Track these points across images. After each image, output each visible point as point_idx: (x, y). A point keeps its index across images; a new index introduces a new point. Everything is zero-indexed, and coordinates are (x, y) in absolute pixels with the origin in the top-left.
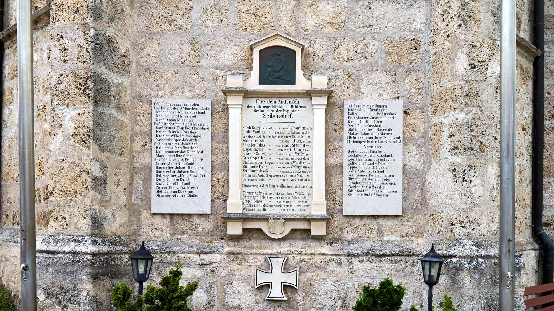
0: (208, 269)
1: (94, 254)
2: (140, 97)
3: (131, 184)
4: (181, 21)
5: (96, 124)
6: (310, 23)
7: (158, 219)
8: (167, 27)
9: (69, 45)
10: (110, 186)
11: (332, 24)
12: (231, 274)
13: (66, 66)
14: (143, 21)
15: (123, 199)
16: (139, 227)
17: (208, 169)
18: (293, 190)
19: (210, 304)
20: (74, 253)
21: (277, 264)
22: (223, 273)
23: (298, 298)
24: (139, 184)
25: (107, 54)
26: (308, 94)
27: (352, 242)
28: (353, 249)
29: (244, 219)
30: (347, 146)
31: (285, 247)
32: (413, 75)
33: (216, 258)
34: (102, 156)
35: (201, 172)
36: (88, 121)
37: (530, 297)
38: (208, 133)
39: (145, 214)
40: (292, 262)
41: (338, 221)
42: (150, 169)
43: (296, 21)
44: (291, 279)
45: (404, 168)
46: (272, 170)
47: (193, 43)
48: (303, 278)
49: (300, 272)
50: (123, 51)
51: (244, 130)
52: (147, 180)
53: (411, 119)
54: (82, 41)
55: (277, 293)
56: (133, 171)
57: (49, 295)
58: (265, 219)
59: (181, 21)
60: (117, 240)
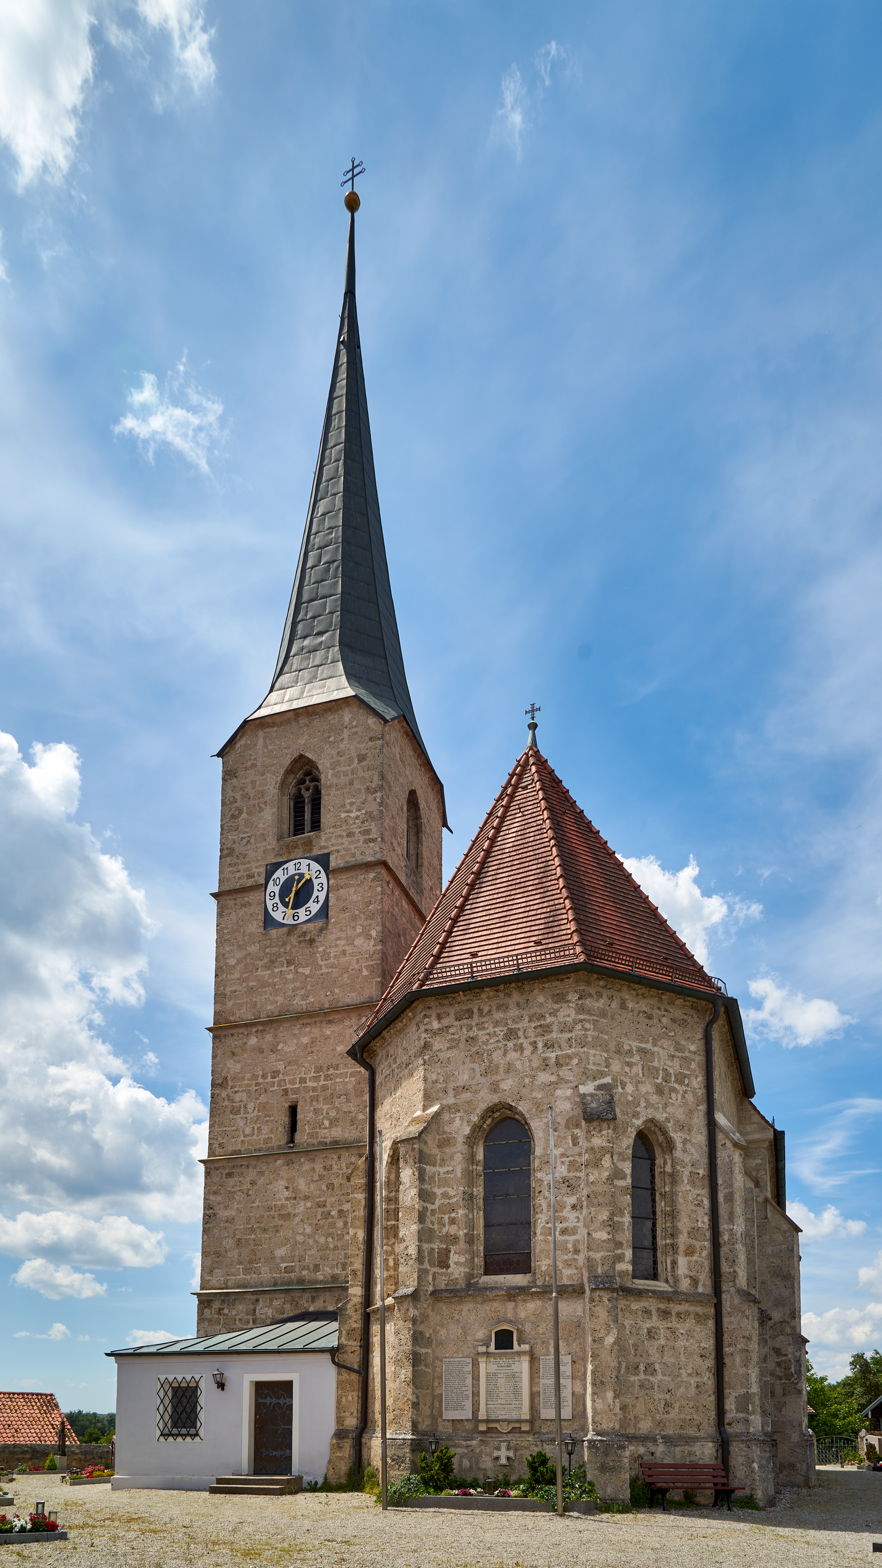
0: (470, 1449)
1: (412, 1440)
2: (437, 1358)
3: (433, 1404)
4: (457, 1317)
5: (414, 1376)
6: (522, 1315)
7: (446, 1423)
8: (450, 1321)
9: (402, 1337)
10: (421, 1406)
11: (534, 1315)
12: (481, 1451)
13: (401, 1348)
14: (438, 1318)
15: (428, 1412)
16: (437, 1426)
17: (471, 1395)
18: (513, 1406)
19: (471, 1467)
20: (404, 1439)
21: (504, 1446)
22: (478, 1451)
23: (515, 1464)
24: (437, 1404)
25: (419, 1340)
26: (519, 1354)
27: (544, 1434)
28: (545, 1437)
29: (487, 1421)
30: (542, 1381)
31: (510, 1437)
32: (578, 1341)
33: (474, 1443)
34: (417, 1391)
35: (467, 1396)
36: (410, 1374)
37: (278, 1453)
38: (470, 1376)
39: (440, 1420)
40: (512, 1445)
41: (538, 1423)
42: (442, 1395)
43: (515, 1313)
44: (511, 1454)
45: (573, 1394)
46: (502, 1395)
47: (463, 1328)
48: (518, 1454)
49: (516, 1450)
50: (428, 1336)
51: (488, 1374)
52: (441, 1402)
53: (577, 1365)
54: (408, 1336)
55: (503, 1461)
56: (434, 1397)
57: (393, 1460)
58: (498, 1421)
59: (457, 1317)
60: (424, 1433)
